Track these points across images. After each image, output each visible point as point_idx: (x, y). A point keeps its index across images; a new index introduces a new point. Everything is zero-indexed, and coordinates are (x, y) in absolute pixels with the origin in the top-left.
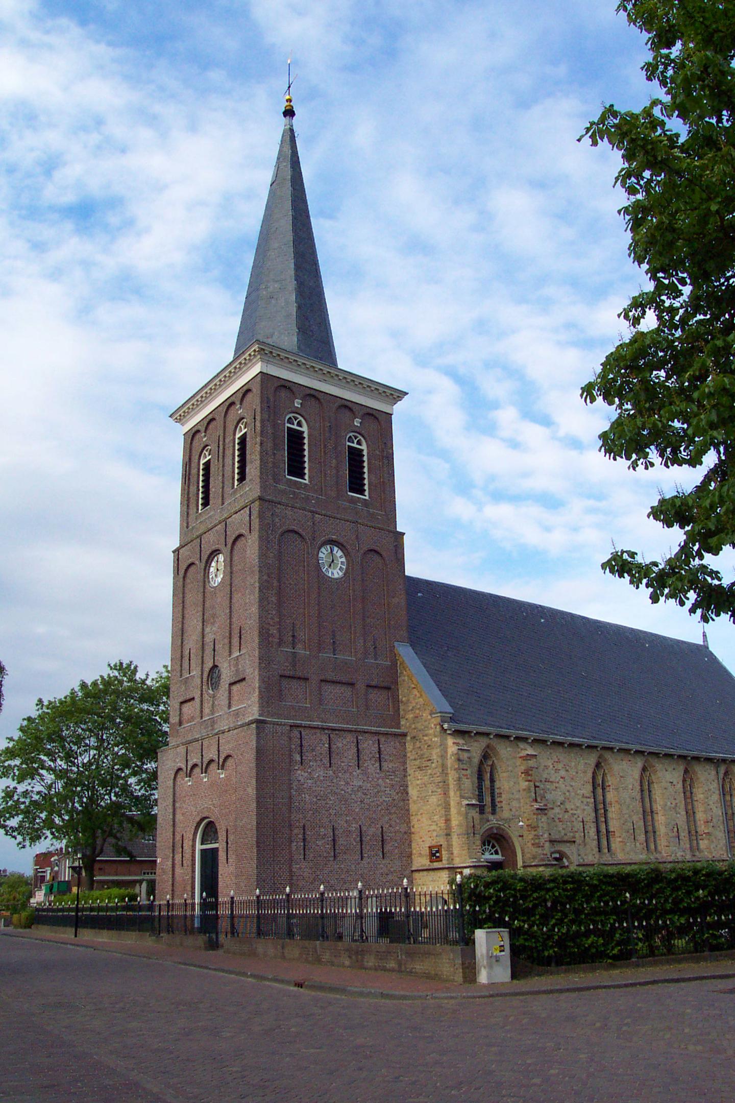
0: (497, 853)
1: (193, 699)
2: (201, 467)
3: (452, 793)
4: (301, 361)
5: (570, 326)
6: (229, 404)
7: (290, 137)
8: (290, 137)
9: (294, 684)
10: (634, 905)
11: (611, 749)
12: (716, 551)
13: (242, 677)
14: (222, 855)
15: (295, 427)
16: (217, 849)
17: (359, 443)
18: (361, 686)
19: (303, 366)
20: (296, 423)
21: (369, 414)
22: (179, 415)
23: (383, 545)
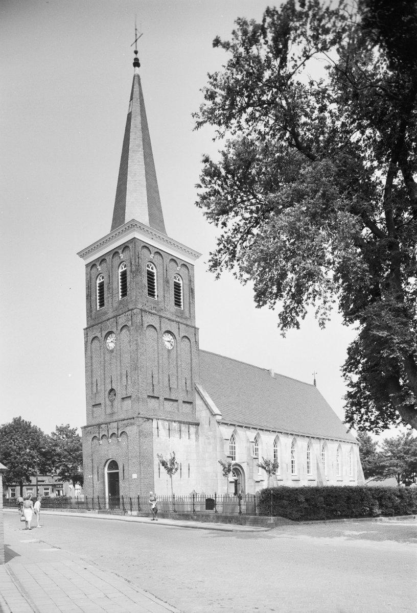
0: (235, 476)
1: (100, 404)
2: (98, 285)
3: (218, 448)
4: (150, 231)
5: (356, 372)
6: (115, 253)
7: (137, 79)
8: (137, 79)
9: (153, 400)
10: (400, 413)
11: (281, 433)
12: (359, 378)
13: (177, 399)
14: (121, 475)
15: (150, 269)
16: (118, 473)
17: (179, 280)
18: (161, 398)
19: (151, 234)
20: (151, 267)
21: (184, 265)
22: (83, 254)
23: (191, 335)
